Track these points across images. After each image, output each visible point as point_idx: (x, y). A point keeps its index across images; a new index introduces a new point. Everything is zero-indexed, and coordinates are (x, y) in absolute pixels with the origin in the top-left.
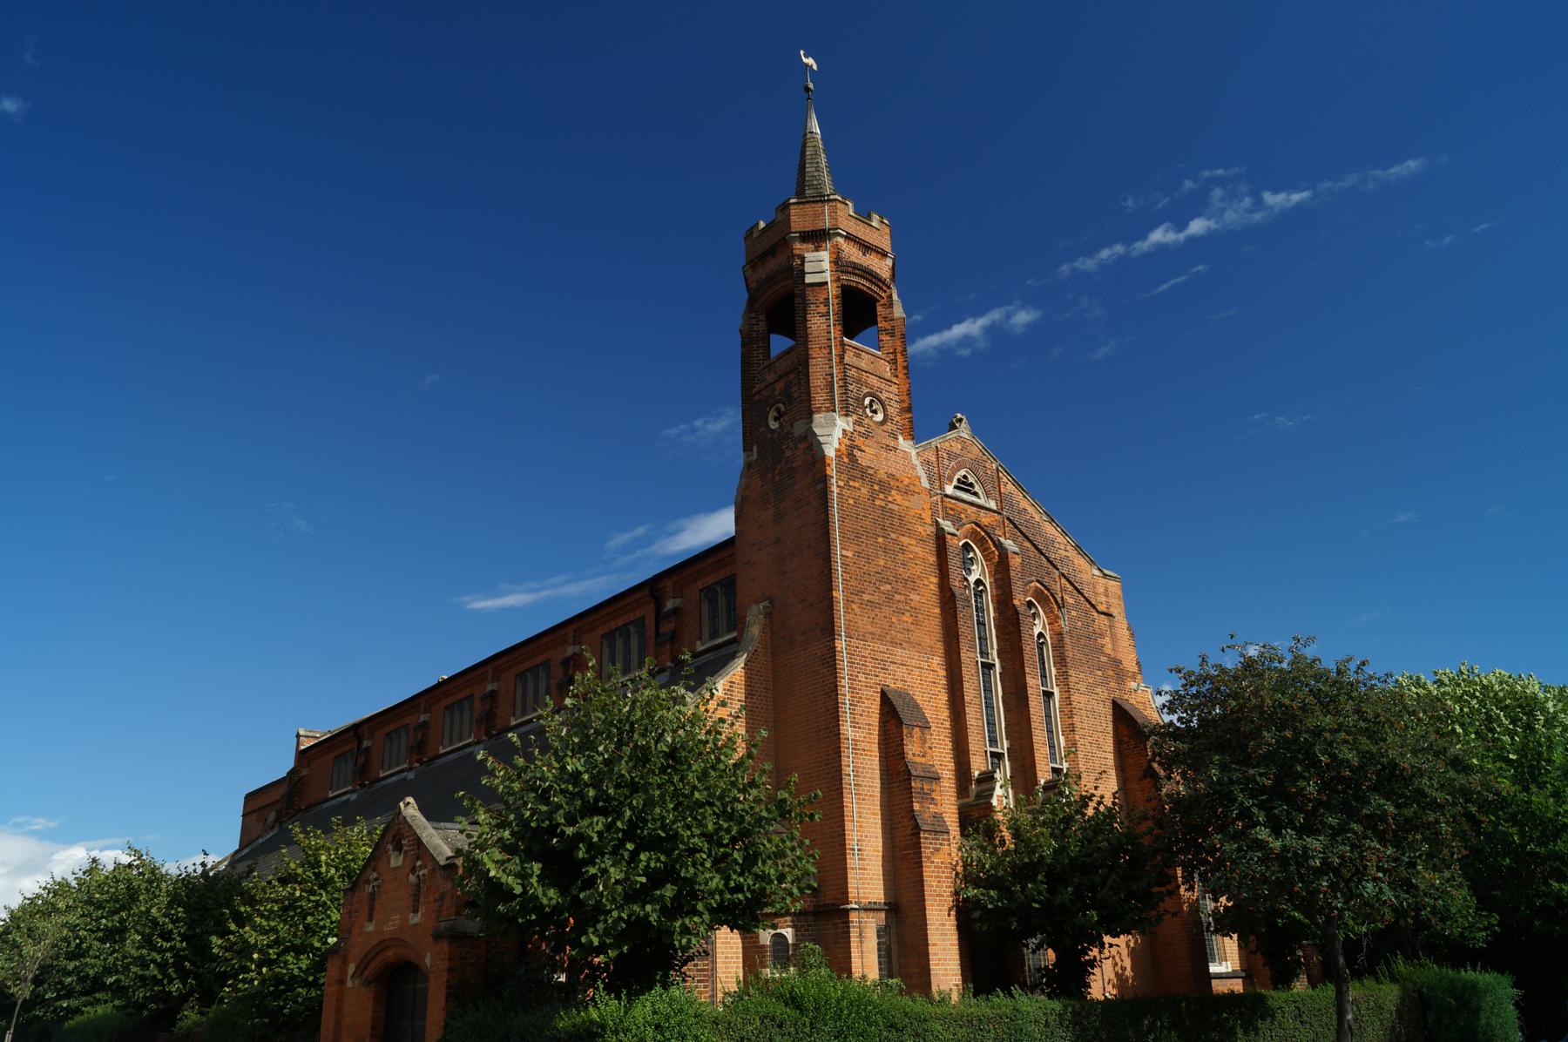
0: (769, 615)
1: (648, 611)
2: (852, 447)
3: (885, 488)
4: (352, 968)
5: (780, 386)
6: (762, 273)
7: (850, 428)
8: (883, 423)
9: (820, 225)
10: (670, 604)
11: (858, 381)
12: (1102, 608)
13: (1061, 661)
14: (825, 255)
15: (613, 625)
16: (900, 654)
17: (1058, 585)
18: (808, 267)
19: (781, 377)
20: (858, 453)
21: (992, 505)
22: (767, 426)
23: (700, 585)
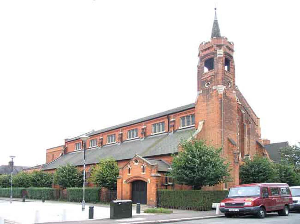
0: (204, 123)
1: (166, 121)
2: (225, 92)
3: (230, 101)
4: (124, 181)
5: (209, 78)
6: (206, 53)
7: (225, 88)
8: (231, 87)
9: (221, 44)
10: (172, 120)
11: (227, 79)
12: (257, 124)
13: (249, 134)
14: (222, 50)
15: (156, 122)
16: (231, 132)
17: (250, 120)
18: (218, 53)
19: (209, 77)
20: (226, 94)
21: (241, 104)
22: (205, 86)
23: (180, 116)
